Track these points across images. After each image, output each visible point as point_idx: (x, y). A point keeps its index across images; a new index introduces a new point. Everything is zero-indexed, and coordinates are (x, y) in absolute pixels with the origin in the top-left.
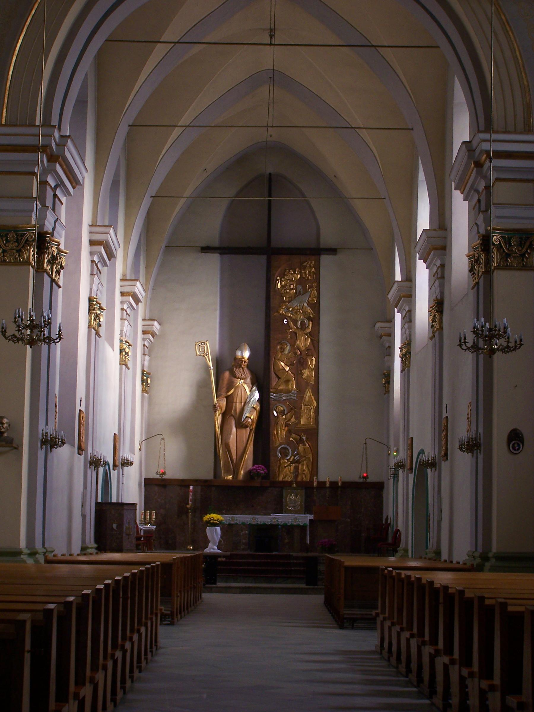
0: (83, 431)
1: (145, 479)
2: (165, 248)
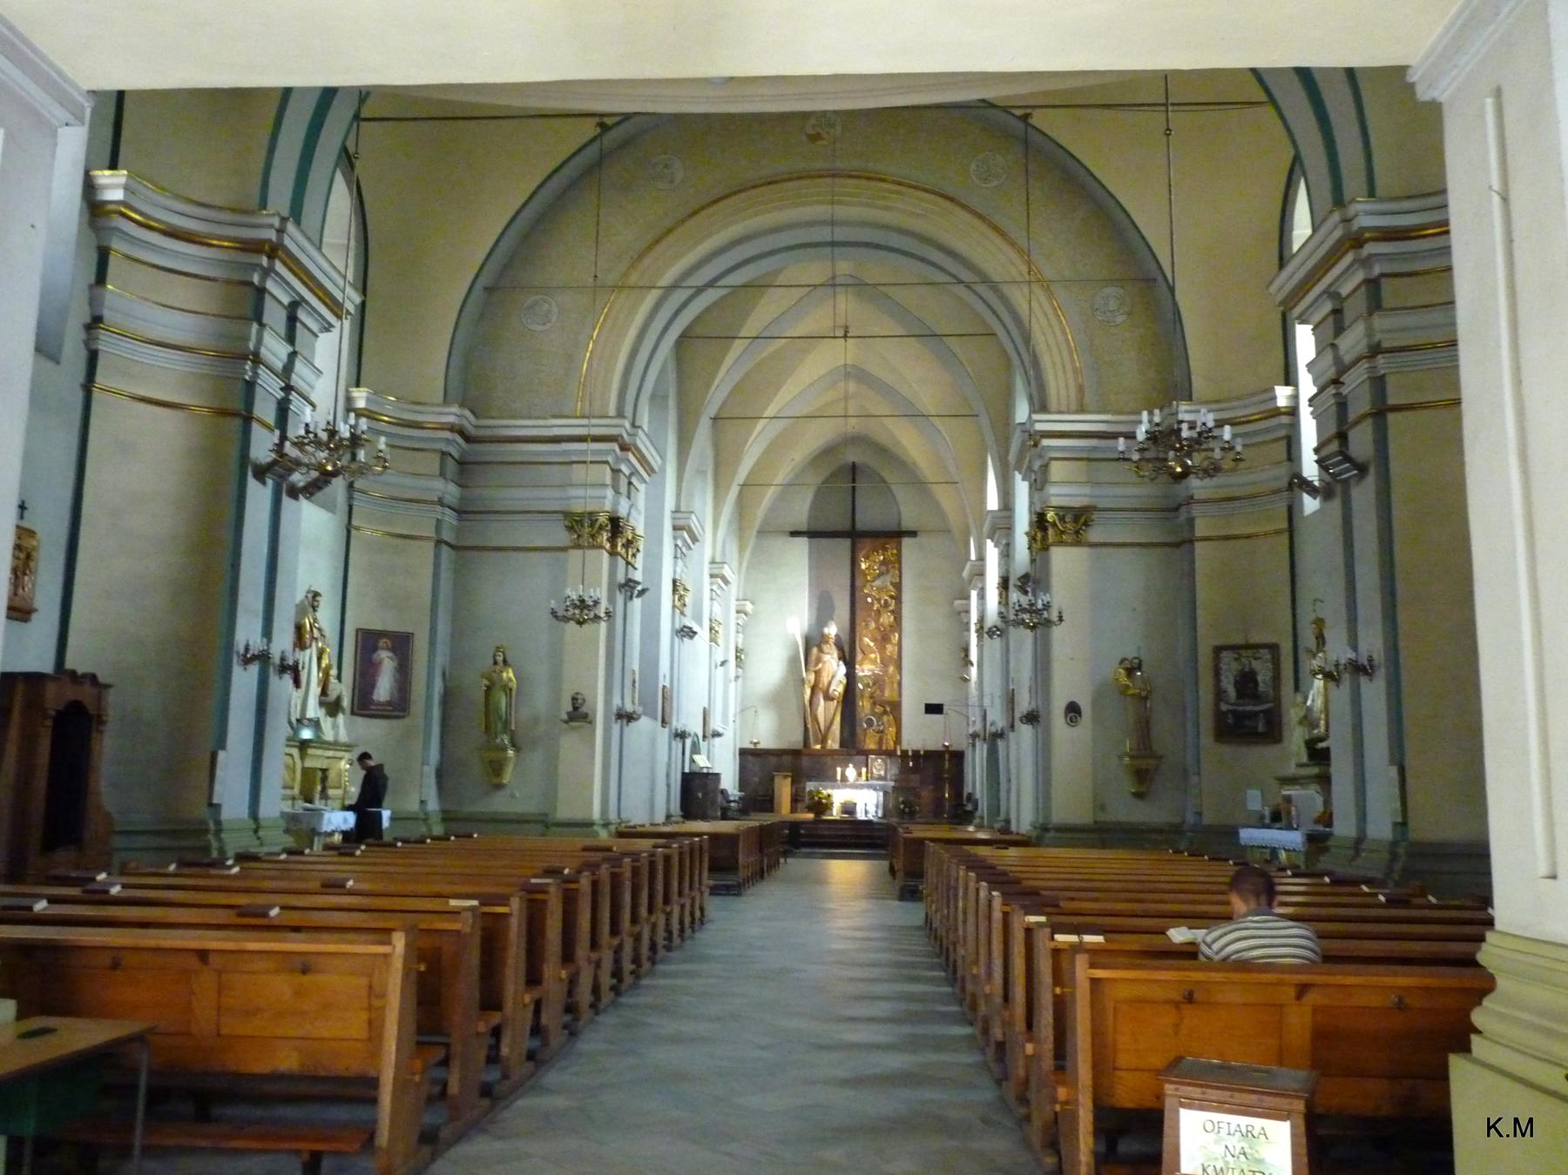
2: (757, 532)
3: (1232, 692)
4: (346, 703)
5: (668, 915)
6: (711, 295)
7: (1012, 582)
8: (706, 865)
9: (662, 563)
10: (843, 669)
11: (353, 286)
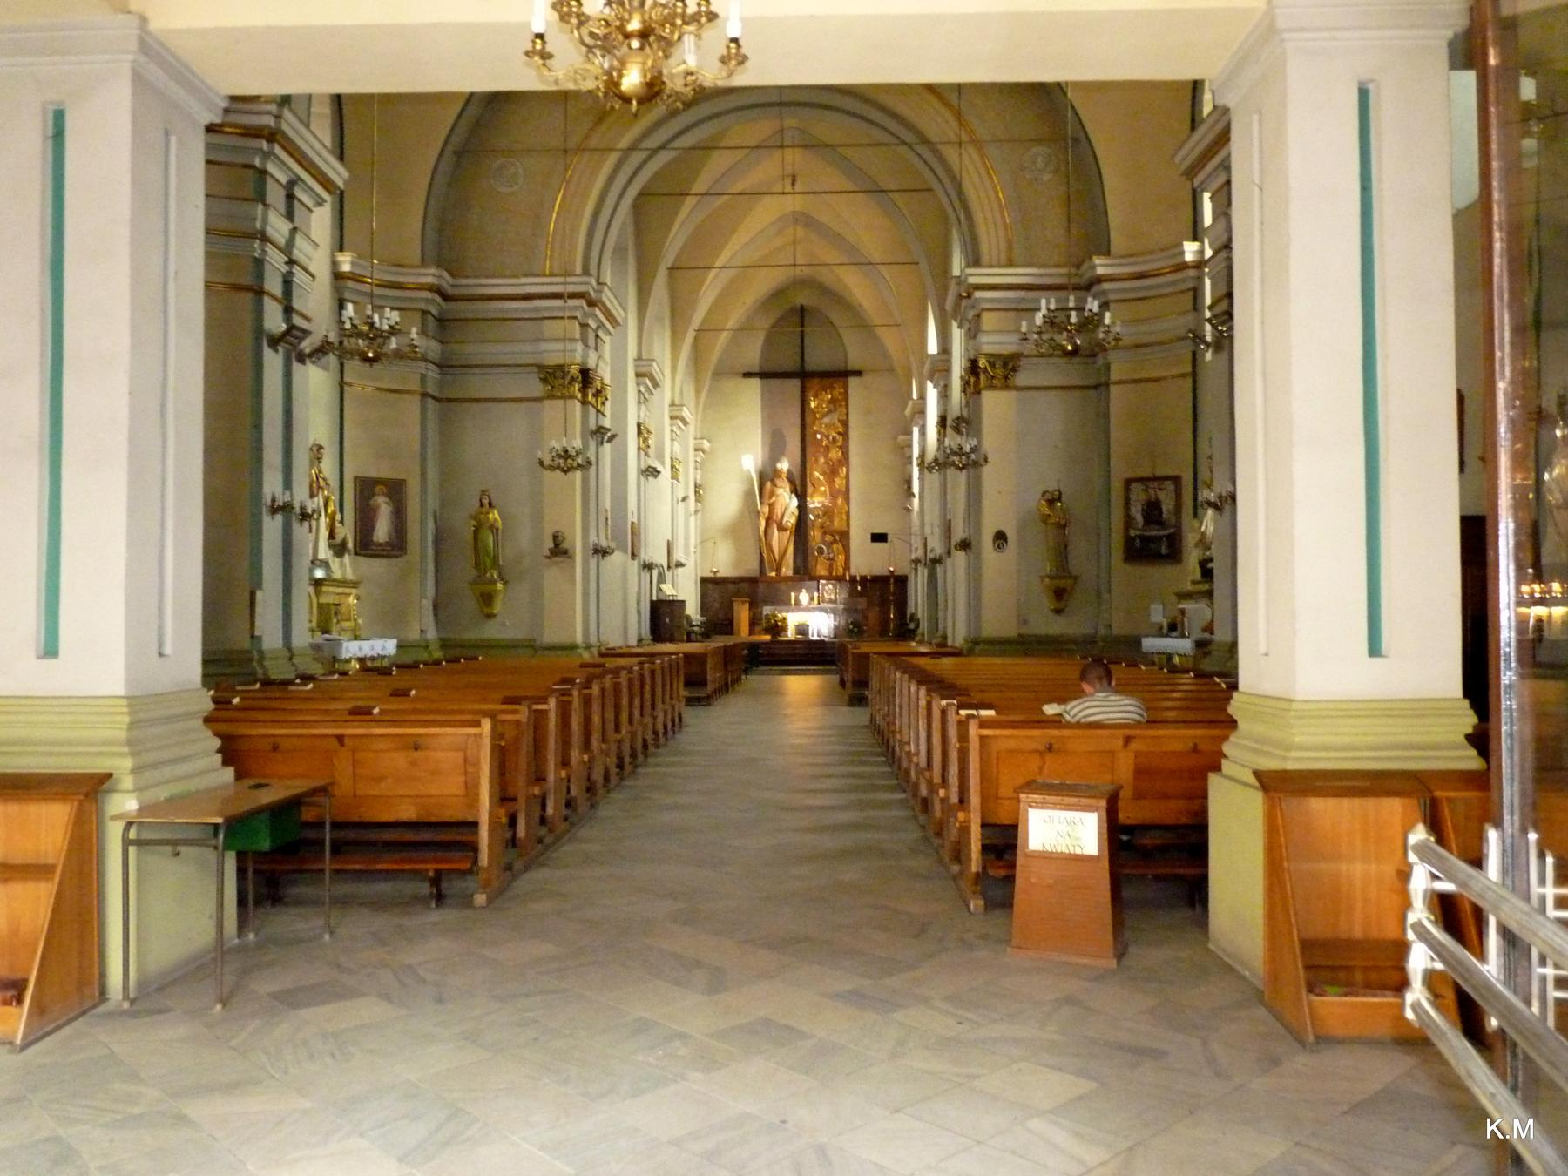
2: (712, 374)
3: (1139, 518)
4: (350, 545)
5: (655, 718)
7: (949, 422)
8: (682, 679)
9: (627, 409)
10: (795, 502)
11: (332, 152)
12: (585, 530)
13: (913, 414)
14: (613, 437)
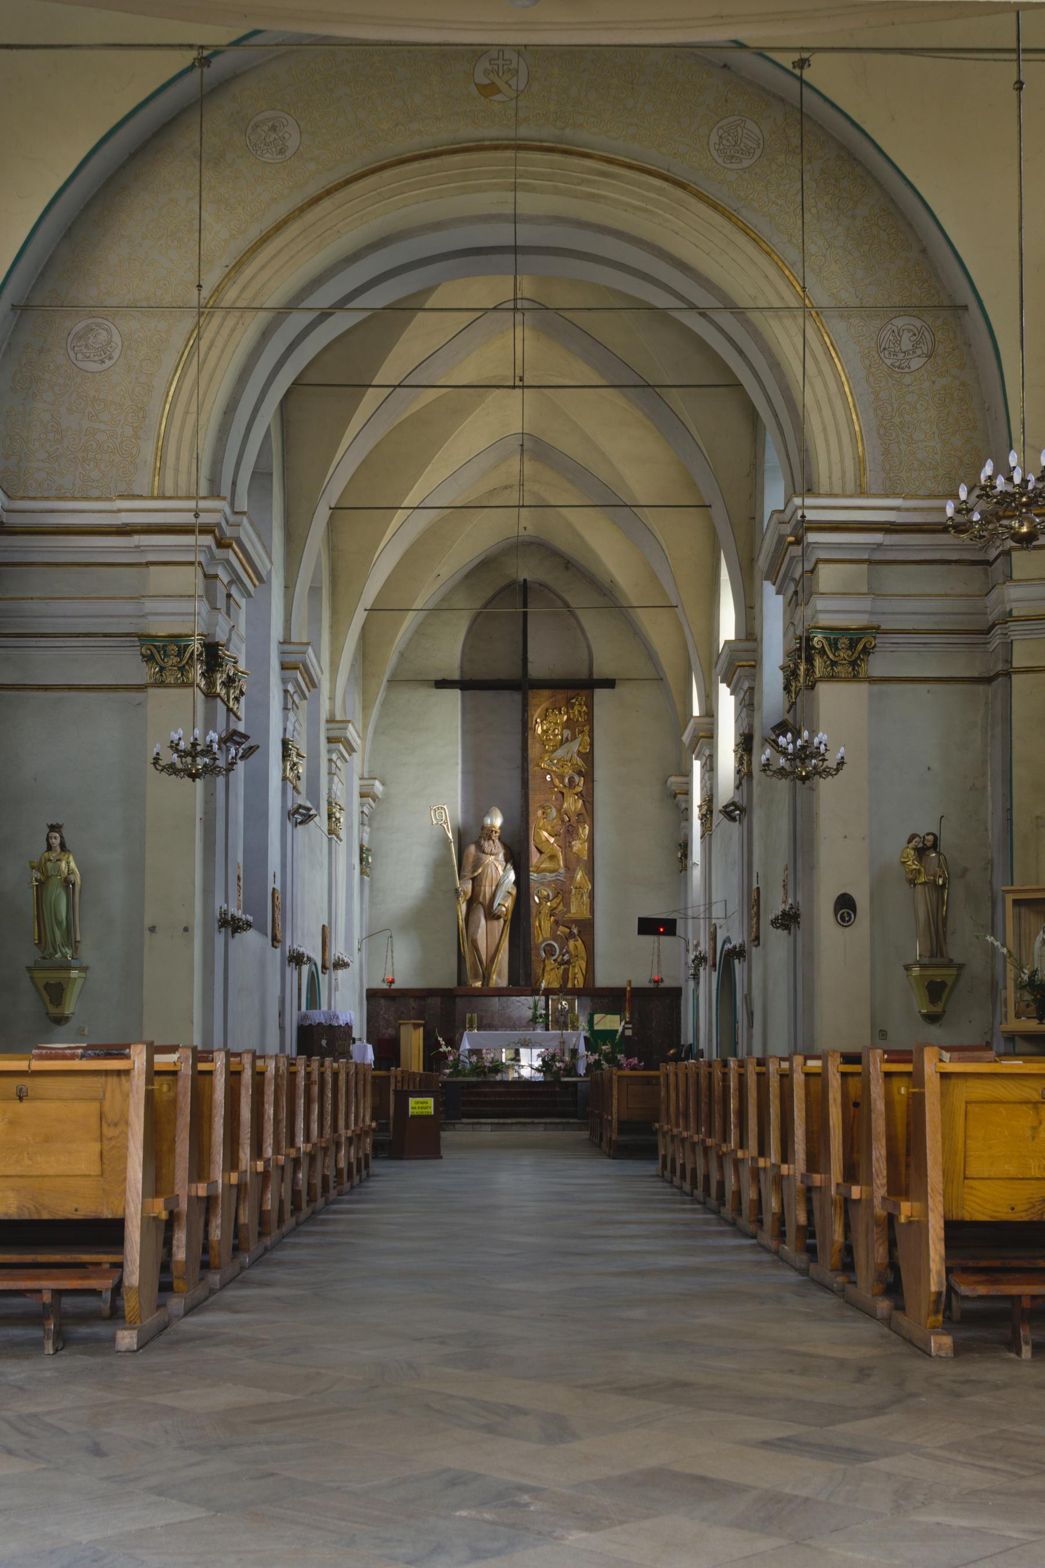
0: (278, 917)
1: (368, 990)
6: (340, 324)
12: (208, 891)
13: (696, 739)
14: (251, 750)
